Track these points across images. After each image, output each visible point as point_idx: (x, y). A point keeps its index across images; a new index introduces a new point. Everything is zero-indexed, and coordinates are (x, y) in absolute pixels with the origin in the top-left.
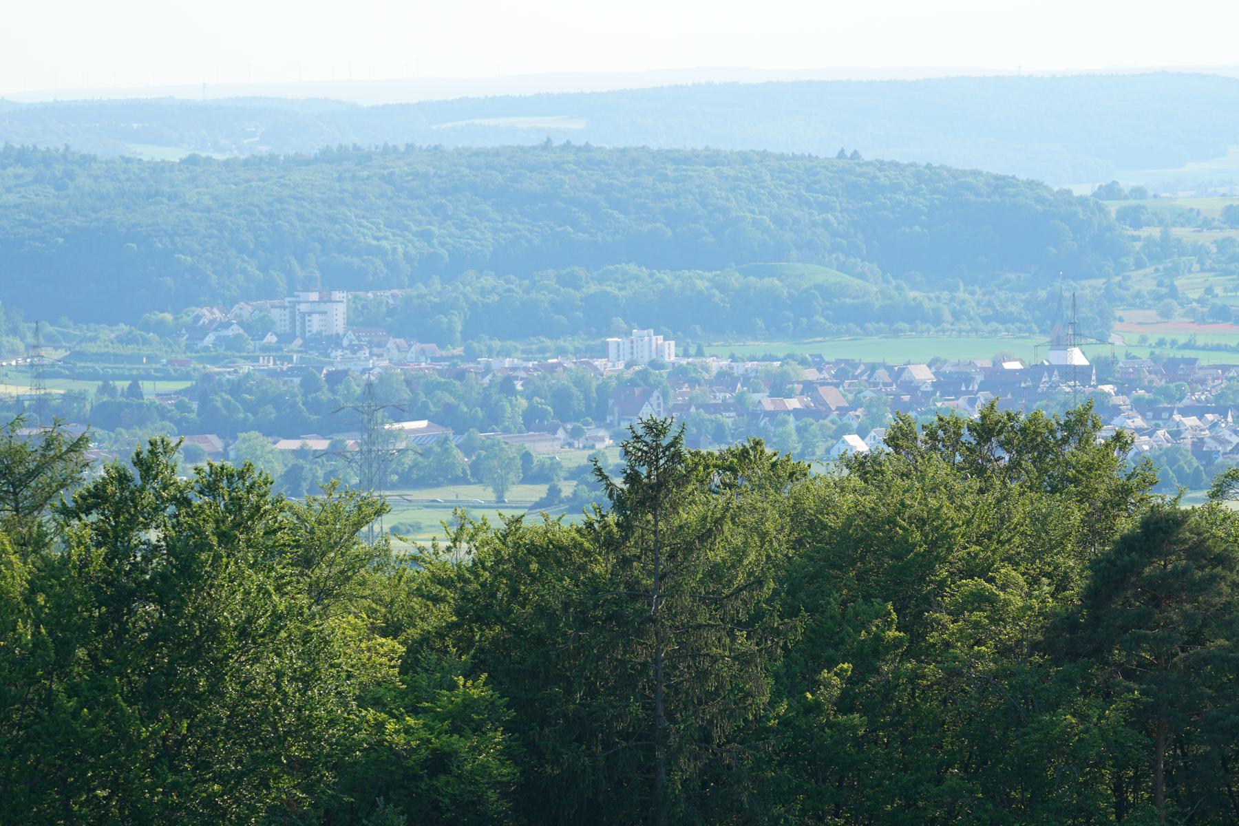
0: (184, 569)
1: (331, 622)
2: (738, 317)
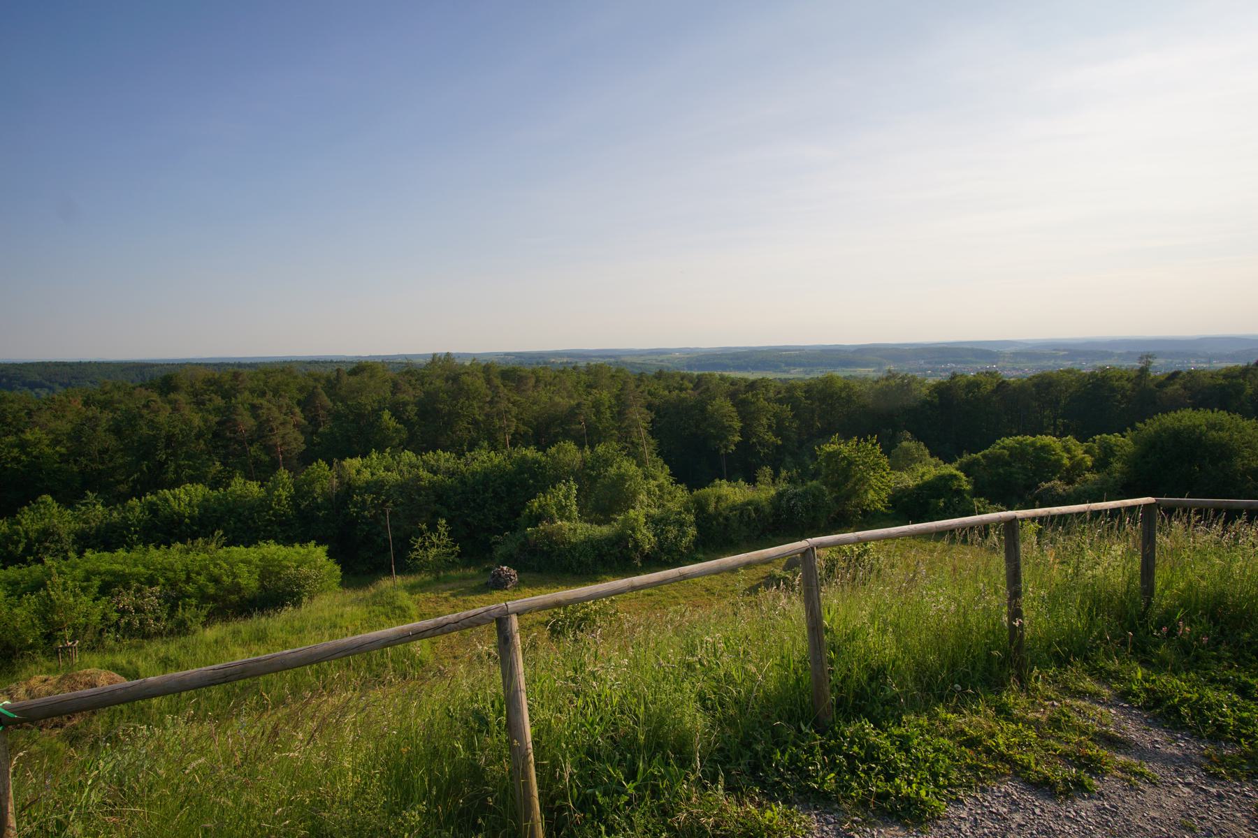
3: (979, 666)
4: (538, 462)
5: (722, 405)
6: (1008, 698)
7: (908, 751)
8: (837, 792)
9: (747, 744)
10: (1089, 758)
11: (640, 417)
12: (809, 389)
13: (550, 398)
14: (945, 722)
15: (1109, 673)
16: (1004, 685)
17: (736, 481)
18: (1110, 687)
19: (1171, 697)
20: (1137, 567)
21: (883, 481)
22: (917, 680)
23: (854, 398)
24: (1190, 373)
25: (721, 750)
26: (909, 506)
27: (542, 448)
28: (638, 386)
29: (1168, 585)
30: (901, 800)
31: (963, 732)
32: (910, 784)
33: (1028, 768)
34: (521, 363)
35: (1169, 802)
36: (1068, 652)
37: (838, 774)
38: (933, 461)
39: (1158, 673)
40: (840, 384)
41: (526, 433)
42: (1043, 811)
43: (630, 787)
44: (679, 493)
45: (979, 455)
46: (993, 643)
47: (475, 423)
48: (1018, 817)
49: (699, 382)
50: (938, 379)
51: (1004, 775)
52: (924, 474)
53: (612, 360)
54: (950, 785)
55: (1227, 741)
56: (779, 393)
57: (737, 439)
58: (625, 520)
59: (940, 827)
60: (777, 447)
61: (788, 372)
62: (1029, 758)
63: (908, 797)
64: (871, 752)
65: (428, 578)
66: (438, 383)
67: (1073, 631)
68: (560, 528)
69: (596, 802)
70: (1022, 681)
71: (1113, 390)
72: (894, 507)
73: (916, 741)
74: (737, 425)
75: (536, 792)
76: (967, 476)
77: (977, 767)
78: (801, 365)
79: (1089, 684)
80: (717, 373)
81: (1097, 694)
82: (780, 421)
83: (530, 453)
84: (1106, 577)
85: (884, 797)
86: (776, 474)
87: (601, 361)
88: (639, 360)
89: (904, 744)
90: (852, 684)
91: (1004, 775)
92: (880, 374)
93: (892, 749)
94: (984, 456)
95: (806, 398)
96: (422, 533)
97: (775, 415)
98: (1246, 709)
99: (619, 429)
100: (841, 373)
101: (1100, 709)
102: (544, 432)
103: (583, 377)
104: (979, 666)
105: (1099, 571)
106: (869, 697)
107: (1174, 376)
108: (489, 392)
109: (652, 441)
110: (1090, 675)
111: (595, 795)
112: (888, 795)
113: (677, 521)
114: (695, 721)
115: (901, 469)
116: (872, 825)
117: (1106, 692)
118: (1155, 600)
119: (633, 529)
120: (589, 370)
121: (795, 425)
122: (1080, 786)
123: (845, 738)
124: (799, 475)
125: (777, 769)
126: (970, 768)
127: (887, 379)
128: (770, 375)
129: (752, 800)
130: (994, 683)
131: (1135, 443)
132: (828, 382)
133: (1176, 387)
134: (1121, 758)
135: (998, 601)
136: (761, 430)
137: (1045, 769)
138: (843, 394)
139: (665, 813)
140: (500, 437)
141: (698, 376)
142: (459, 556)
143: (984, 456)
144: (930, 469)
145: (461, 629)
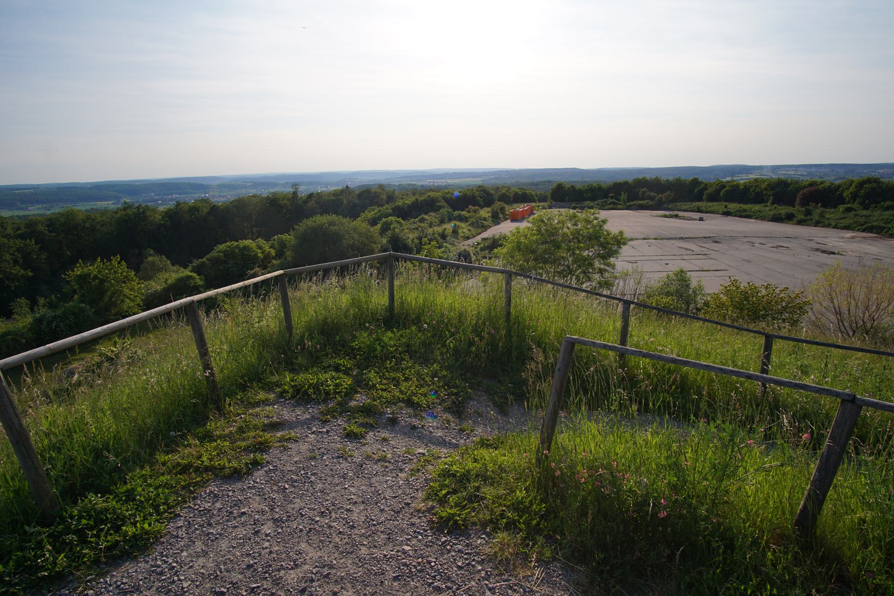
0: (144, 212)
1: (373, 301)
2: (183, 193)
7: (134, 500)
8: (70, 566)
10: (261, 443)
12: (51, 223)
18: (274, 393)
19: (304, 386)
20: (283, 314)
23: (98, 227)
24: (318, 194)
31: (178, 464)
35: (304, 447)
36: (251, 379)
38: (175, 268)
39: (298, 374)
42: (234, 491)
45: (204, 259)
51: (208, 481)
54: (169, 508)
56: (18, 229)
59: (163, 543)
61: (26, 209)
62: (224, 462)
63: (134, 536)
64: (99, 518)
70: (219, 409)
73: (139, 489)
76: (199, 275)
77: (189, 485)
78: (38, 202)
79: (262, 396)
89: (130, 496)
92: (119, 206)
93: (118, 506)
95: (50, 232)
97: (19, 250)
98: (338, 378)
100: (82, 207)
105: (264, 323)
112: (117, 542)
116: (104, 575)
117: (272, 396)
122: (256, 464)
126: (184, 488)
127: (124, 209)
131: (296, 238)
132: (69, 216)
133: (312, 203)
134: (279, 434)
137: (234, 464)
138: (87, 225)
143: (207, 259)
144: (174, 274)
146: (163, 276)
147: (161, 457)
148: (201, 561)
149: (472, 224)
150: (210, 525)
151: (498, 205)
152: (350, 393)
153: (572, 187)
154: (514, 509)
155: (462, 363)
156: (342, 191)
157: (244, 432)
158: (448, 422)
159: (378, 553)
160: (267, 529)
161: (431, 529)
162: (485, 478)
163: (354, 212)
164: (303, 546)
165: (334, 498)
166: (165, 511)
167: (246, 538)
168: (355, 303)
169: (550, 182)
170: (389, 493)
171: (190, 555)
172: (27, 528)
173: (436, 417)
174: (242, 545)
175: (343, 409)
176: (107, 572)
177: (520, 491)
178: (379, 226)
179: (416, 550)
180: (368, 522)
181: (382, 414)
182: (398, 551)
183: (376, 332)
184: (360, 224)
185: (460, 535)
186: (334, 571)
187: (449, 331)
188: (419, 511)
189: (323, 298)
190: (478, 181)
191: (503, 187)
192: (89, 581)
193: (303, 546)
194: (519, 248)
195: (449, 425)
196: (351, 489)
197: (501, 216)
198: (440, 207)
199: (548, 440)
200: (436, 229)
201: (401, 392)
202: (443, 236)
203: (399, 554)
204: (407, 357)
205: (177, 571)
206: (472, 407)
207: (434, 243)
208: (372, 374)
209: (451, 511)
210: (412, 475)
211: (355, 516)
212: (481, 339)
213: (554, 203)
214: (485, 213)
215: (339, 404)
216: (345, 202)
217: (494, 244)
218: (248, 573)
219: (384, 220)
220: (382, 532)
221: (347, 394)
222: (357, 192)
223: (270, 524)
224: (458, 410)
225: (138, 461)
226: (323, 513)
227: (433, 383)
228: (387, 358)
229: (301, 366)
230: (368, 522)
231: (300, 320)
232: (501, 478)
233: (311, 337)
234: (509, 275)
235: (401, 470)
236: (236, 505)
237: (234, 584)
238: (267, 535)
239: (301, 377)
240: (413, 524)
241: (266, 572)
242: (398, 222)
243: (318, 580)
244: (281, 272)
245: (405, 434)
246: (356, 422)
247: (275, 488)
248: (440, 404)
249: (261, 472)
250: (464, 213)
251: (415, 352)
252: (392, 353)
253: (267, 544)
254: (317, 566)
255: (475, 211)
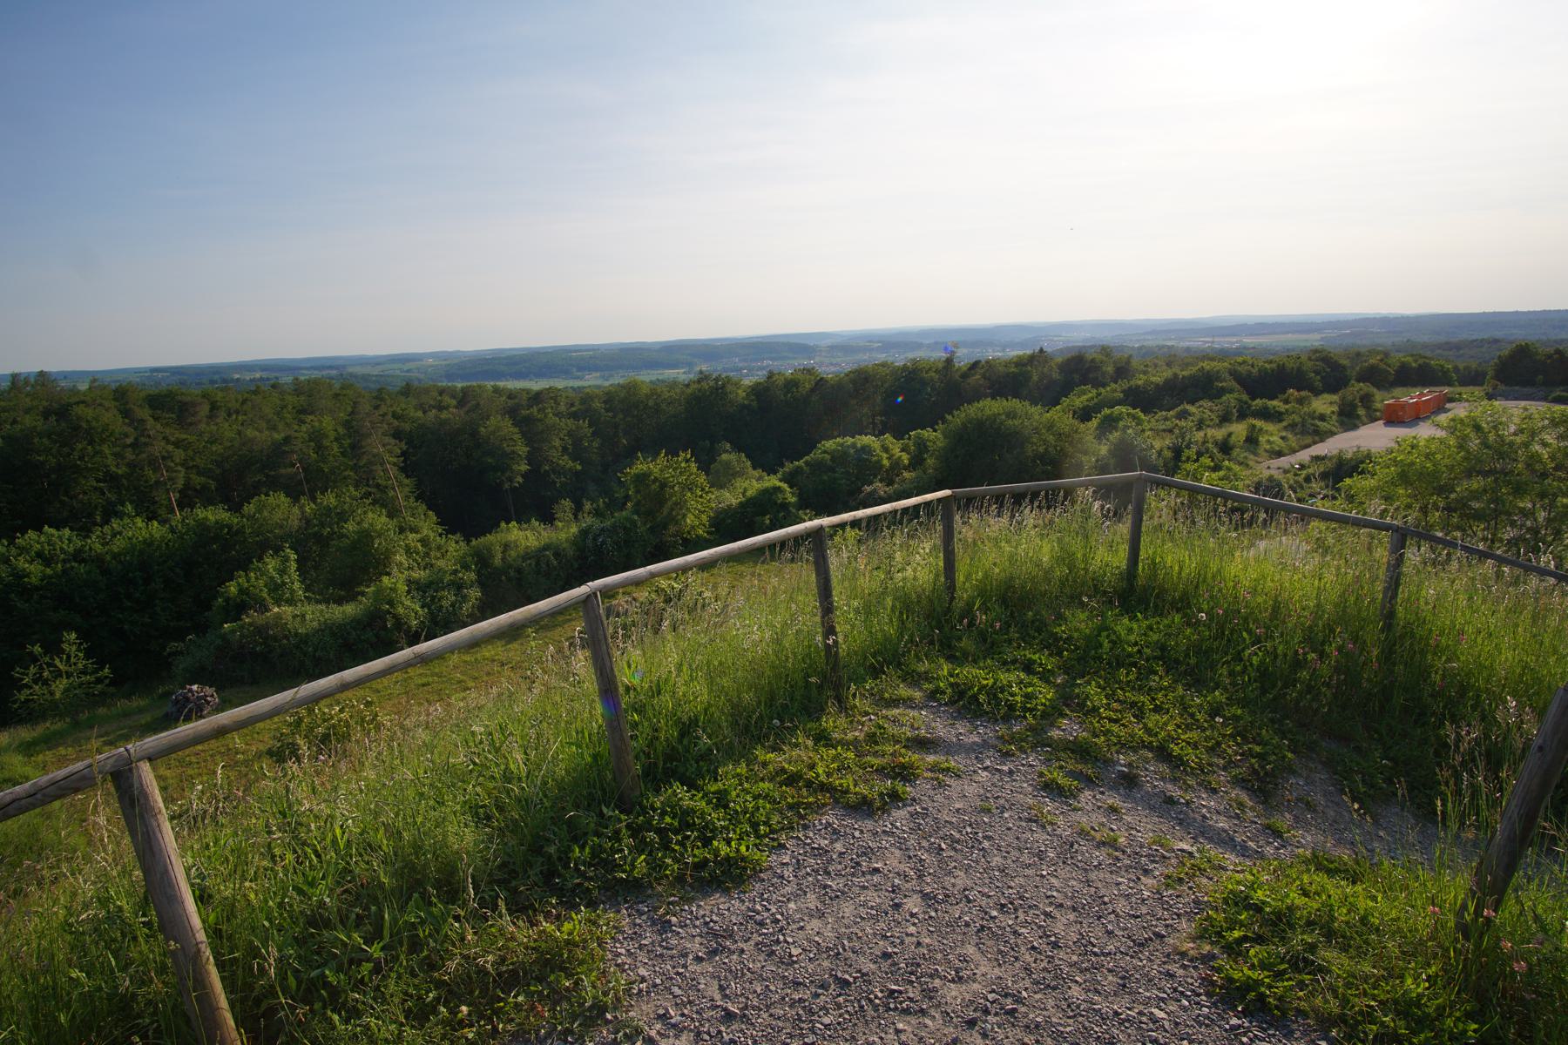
3: (798, 695)
4: (230, 527)
5: (500, 426)
6: (827, 723)
7: (726, 807)
9: (537, 849)
10: (903, 767)
11: (384, 450)
12: (609, 398)
13: (239, 433)
14: (765, 764)
15: (919, 675)
16: (823, 710)
17: (528, 521)
18: (921, 689)
19: (971, 688)
20: (941, 564)
21: (701, 503)
22: (734, 724)
23: (664, 406)
24: (988, 362)
25: (504, 865)
26: (729, 526)
27: (235, 508)
28: (377, 407)
29: (968, 577)
30: (721, 863)
31: (783, 770)
32: (728, 843)
33: (847, 792)
34: (183, 383)
35: (972, 790)
36: (885, 660)
37: (650, 854)
38: (756, 473)
39: (961, 665)
40: (645, 390)
41: (204, 487)
43: (375, 951)
44: (452, 546)
45: (801, 463)
46: (810, 666)
47: (111, 478)
48: (839, 846)
49: (464, 398)
50: (754, 379)
51: (824, 805)
52: (745, 490)
53: (334, 372)
54: (772, 831)
55: (1016, 718)
56: (572, 405)
57: (524, 467)
58: (379, 591)
60: (577, 473)
61: (581, 378)
62: (848, 782)
63: (727, 858)
64: (685, 819)
65: (59, 726)
66: (28, 421)
67: (887, 639)
68: (278, 616)
69: (326, 985)
70: (840, 700)
71: (924, 383)
72: (718, 530)
73: (734, 794)
74: (522, 450)
75: (223, 1002)
77: (798, 805)
78: (596, 369)
79: (903, 691)
80: (489, 384)
81: (911, 699)
82: (577, 442)
83: (214, 515)
84: (915, 579)
85: (701, 865)
86: (578, 508)
87: (316, 374)
88: (376, 371)
89: (721, 801)
90: (660, 746)
91: (824, 805)
93: (708, 809)
94: (807, 463)
95: (607, 410)
96: (35, 659)
98: (1030, 684)
99: (355, 468)
100: (646, 377)
101: (912, 713)
102: (235, 480)
103: (289, 398)
104: (798, 695)
105: (909, 572)
106: (681, 756)
107: (975, 365)
108: (130, 430)
109: (407, 481)
110: (904, 681)
111: (323, 976)
112: (706, 861)
113: (452, 583)
114: (463, 837)
115: (722, 487)
116: (690, 901)
117: (918, 694)
118: (958, 593)
119: (391, 603)
120: (299, 389)
121: (595, 444)
122: (895, 797)
123: (654, 810)
124: (608, 506)
125: (577, 869)
128: (560, 384)
129: (547, 915)
130: (812, 710)
131: (945, 437)
132: (631, 388)
133: (976, 378)
134: (931, 759)
135: (810, 620)
136: (554, 455)
137: (863, 789)
138: (651, 403)
139: (433, 967)
140: (160, 496)
141: (463, 389)
142: (113, 683)
143: (807, 463)
144: (753, 483)
145: (44, 803)
146: (740, 484)
147: (760, 754)
148: (815, 924)
149: (1292, 427)
150: (827, 873)
151: (1356, 389)
152: (1051, 715)
153: (1558, 352)
154: (1398, 1013)
155: (1275, 699)
156: (1032, 358)
157: (876, 743)
158: (1241, 805)
159: (1101, 1004)
160: (913, 904)
161: (1208, 994)
162: (1329, 934)
163: (1051, 395)
164: (970, 950)
165: (1022, 886)
166: (766, 835)
167: (881, 912)
168: (1066, 558)
169: (1496, 341)
170: (1121, 906)
171: (798, 910)
172: (605, 810)
173: (1214, 791)
174: (876, 919)
175: (1037, 740)
176: (693, 899)
177: (1416, 979)
178: (1094, 423)
179: (1177, 1024)
180: (1084, 944)
181: (1109, 763)
182: (1141, 1013)
183: (1103, 614)
184: (1060, 416)
185: (1271, 1025)
186: (1023, 1009)
187: (1250, 632)
188: (1183, 954)
189: (1009, 543)
190: (1314, 340)
191: (1372, 352)
192: (671, 903)
193: (970, 950)
194: (1404, 478)
195: (1243, 812)
196: (1053, 880)
197: (1361, 412)
198: (1222, 392)
199: (1493, 888)
200: (1210, 432)
201: (1148, 731)
202: (1225, 447)
203: (1144, 1019)
204: (1160, 670)
205: (782, 929)
206: (1294, 786)
207: (1206, 461)
208: (1092, 689)
209: (1255, 975)
210: (1168, 885)
211: (1059, 928)
212: (1322, 655)
213: (1502, 387)
214: (1324, 404)
215: (1031, 728)
216: (1035, 378)
217: (1340, 470)
218: (885, 965)
219: (1107, 411)
220: (1110, 971)
221: (1044, 715)
222: (1060, 360)
223: (916, 898)
224: (1263, 786)
225: (732, 754)
226: (1003, 906)
227: (1212, 727)
228: (1120, 665)
229: (965, 655)
230: (1084, 944)
231: (969, 575)
232: (1366, 942)
233: (985, 609)
234: (1401, 537)
235: (1146, 872)
236: (865, 854)
237: (863, 975)
238: (913, 915)
239: (968, 672)
240: (1171, 976)
241: (911, 973)
242: (1134, 417)
243: (996, 1014)
244: (947, 492)
245: (1153, 808)
246: (1061, 767)
247: (925, 844)
248: (1225, 769)
249: (902, 813)
250: (1275, 403)
251: (1177, 662)
252: (1130, 655)
253: (912, 929)
254: (993, 991)
255: (1300, 401)
